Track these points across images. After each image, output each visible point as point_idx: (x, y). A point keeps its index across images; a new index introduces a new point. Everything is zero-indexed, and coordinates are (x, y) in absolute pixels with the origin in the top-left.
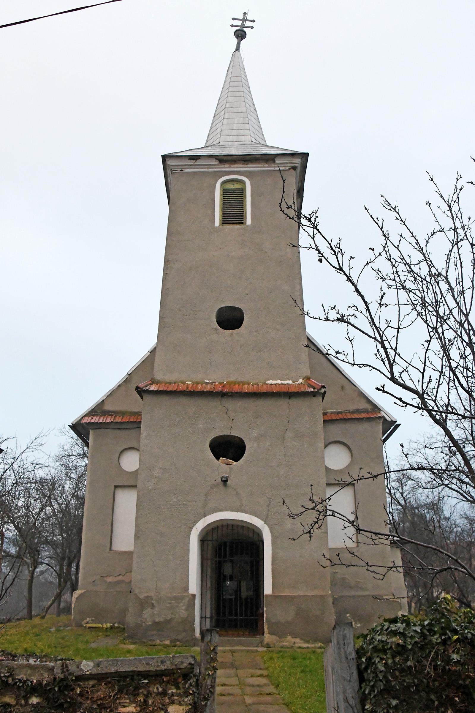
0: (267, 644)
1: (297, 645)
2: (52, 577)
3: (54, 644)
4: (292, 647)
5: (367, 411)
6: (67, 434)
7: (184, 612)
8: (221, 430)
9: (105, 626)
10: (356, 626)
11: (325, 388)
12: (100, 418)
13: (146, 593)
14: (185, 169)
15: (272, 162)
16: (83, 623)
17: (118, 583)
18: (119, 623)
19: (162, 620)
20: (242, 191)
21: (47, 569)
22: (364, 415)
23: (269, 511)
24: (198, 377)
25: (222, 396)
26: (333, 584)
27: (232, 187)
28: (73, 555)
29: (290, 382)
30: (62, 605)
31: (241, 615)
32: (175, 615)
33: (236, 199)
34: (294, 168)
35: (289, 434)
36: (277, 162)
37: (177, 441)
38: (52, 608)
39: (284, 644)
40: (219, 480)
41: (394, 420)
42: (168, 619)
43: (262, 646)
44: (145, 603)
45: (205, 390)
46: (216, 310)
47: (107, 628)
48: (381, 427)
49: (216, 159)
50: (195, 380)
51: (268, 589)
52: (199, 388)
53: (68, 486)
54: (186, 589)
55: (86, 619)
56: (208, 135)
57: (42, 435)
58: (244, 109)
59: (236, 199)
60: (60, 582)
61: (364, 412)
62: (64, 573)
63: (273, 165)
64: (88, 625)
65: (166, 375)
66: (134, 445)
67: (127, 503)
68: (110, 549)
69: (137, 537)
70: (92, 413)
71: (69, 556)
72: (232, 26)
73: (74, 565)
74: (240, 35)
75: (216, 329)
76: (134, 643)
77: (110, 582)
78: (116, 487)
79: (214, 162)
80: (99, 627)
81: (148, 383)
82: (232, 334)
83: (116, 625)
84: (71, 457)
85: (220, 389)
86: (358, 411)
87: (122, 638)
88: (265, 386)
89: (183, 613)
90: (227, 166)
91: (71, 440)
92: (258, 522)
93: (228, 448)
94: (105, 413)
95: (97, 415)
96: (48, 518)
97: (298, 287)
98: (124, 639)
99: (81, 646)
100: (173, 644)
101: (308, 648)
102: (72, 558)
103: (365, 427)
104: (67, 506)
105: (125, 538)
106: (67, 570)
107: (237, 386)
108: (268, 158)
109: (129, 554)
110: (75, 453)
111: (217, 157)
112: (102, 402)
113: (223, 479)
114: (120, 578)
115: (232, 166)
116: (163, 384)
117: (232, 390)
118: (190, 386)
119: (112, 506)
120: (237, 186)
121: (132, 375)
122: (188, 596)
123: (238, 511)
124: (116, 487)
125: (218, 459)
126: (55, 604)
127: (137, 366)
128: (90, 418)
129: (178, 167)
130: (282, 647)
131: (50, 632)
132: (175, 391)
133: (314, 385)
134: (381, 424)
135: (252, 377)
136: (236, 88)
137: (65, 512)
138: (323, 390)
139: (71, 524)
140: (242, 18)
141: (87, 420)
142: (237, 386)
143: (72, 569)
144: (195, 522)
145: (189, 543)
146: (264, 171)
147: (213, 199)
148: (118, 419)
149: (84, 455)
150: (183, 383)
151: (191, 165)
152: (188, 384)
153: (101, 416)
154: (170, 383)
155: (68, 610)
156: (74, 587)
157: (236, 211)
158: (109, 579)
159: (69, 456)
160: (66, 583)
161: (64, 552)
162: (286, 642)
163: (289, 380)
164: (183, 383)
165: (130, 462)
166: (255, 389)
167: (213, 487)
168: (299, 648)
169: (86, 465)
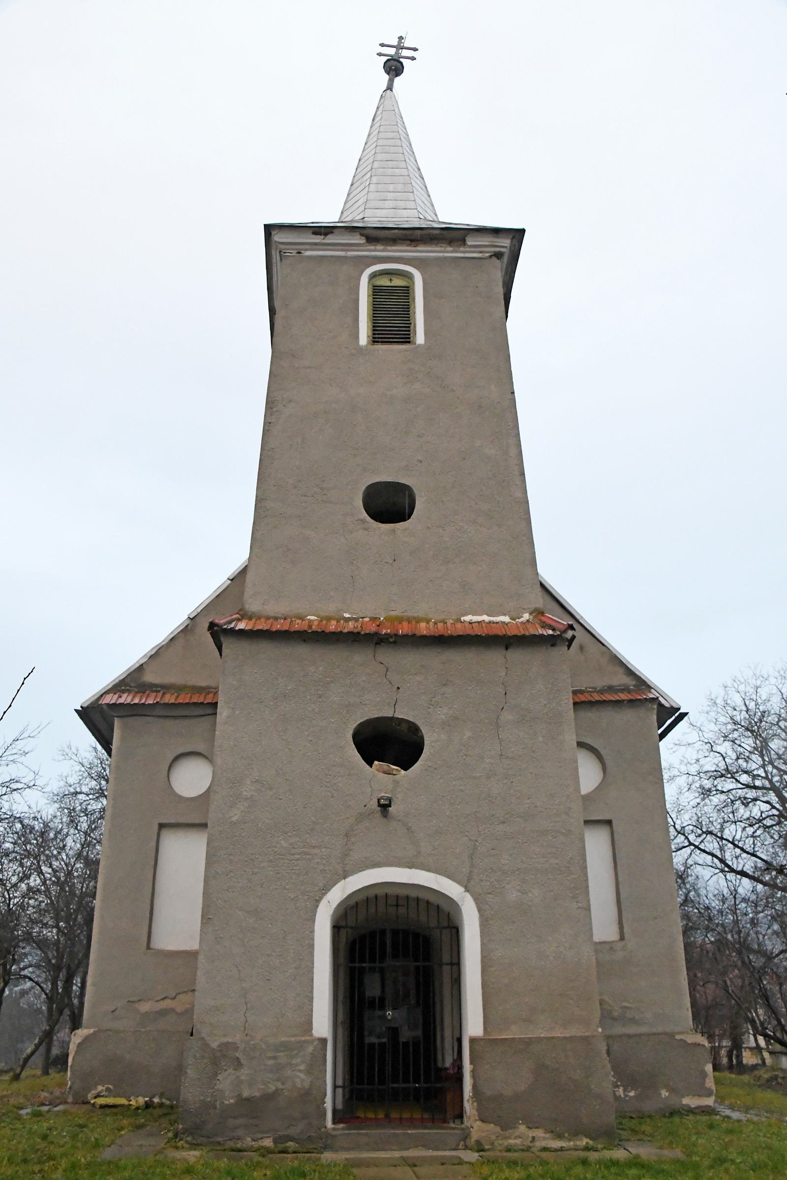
0: (478, 1142)
1: (539, 1144)
2: (39, 1001)
3: (24, 1151)
4: (528, 1149)
5: (625, 689)
6: (74, 757)
7: (302, 1075)
8: (375, 707)
9: (133, 1102)
10: (626, 1096)
11: (573, 629)
12: (134, 697)
13: (225, 1036)
14: (306, 250)
15: (460, 243)
16: (90, 1096)
17: (163, 1013)
18: (161, 1096)
19: (257, 1094)
20: (407, 292)
21: (32, 988)
22: (623, 696)
23: (472, 866)
24: (331, 608)
25: (376, 644)
26: (607, 1017)
27: (389, 284)
28: (76, 962)
29: (506, 619)
30: (55, 1051)
31: (417, 1080)
32: (283, 1084)
33: (392, 316)
34: (498, 255)
35: (507, 716)
36: (469, 243)
37: (291, 729)
38: (33, 1058)
39: (512, 1141)
40: (374, 804)
41: (675, 706)
42: (270, 1091)
43: (466, 1148)
44: (221, 1058)
45: (346, 631)
46: (364, 488)
47: (138, 1108)
48: (655, 717)
49: (362, 235)
50: (323, 614)
51: (474, 1024)
52: (332, 627)
53: (73, 843)
54: (308, 1025)
55: (96, 1088)
56: (342, 213)
57: (26, 735)
58: (405, 172)
59: (392, 316)
60: (50, 1009)
61: (622, 691)
62: (58, 993)
63: (462, 249)
64: (101, 1101)
65: (267, 605)
66: (201, 747)
67: (184, 861)
68: (148, 947)
69: (206, 919)
70: (119, 687)
71: (68, 964)
72: (380, 54)
73: (77, 980)
74: (394, 68)
75: (363, 521)
76: (194, 1146)
77: (146, 1012)
78: (162, 826)
79: (358, 239)
80: (122, 1106)
81: (234, 616)
82: (394, 531)
83: (156, 1100)
84: (80, 796)
85: (373, 628)
86: (610, 689)
87: (170, 1135)
88: (459, 625)
89: (301, 1079)
90: (380, 247)
91: (79, 767)
92: (452, 889)
93: (389, 743)
94: (144, 688)
95: (129, 691)
96: (32, 891)
97: (513, 452)
98: (176, 1135)
99: (82, 1158)
100: (281, 1147)
101: (562, 1149)
102: (73, 966)
103: (627, 716)
104: (69, 874)
105: (179, 924)
106: (64, 988)
107: (405, 624)
108: (454, 236)
109: (191, 956)
110: (85, 789)
111: (365, 232)
112: (140, 669)
113: (382, 802)
114: (167, 1004)
115: (389, 248)
116: (263, 620)
117: (398, 630)
118: (316, 623)
119: (153, 863)
120: (398, 282)
121: (197, 619)
122: (312, 1042)
123: (411, 866)
124: (162, 826)
125: (370, 764)
126: (42, 1049)
127: (207, 602)
128: (116, 696)
129: (293, 247)
130: (508, 1150)
131: (19, 1118)
132: (286, 631)
133: (553, 624)
134: (655, 712)
135: (431, 611)
136: (388, 146)
137: (64, 882)
138: (570, 634)
139: (73, 908)
140: (396, 44)
141: (110, 699)
142: (405, 624)
143: (74, 988)
144: (326, 889)
145: (313, 932)
146: (446, 258)
147: (356, 301)
148: (169, 699)
149: (100, 793)
150: (302, 618)
151: (316, 244)
152: (310, 621)
153: (137, 693)
154: (276, 619)
155: (61, 1061)
156: (76, 1023)
157: (398, 322)
158: (145, 1007)
159: (76, 793)
160: (61, 1013)
161: (60, 957)
162: (516, 1138)
163: (505, 615)
164: (300, 619)
165: (192, 779)
166: (440, 629)
167: (361, 817)
168: (545, 1149)
169: (104, 809)
